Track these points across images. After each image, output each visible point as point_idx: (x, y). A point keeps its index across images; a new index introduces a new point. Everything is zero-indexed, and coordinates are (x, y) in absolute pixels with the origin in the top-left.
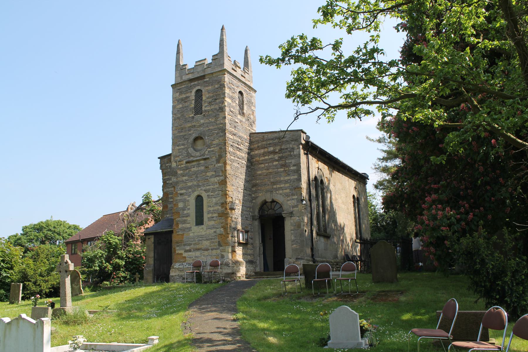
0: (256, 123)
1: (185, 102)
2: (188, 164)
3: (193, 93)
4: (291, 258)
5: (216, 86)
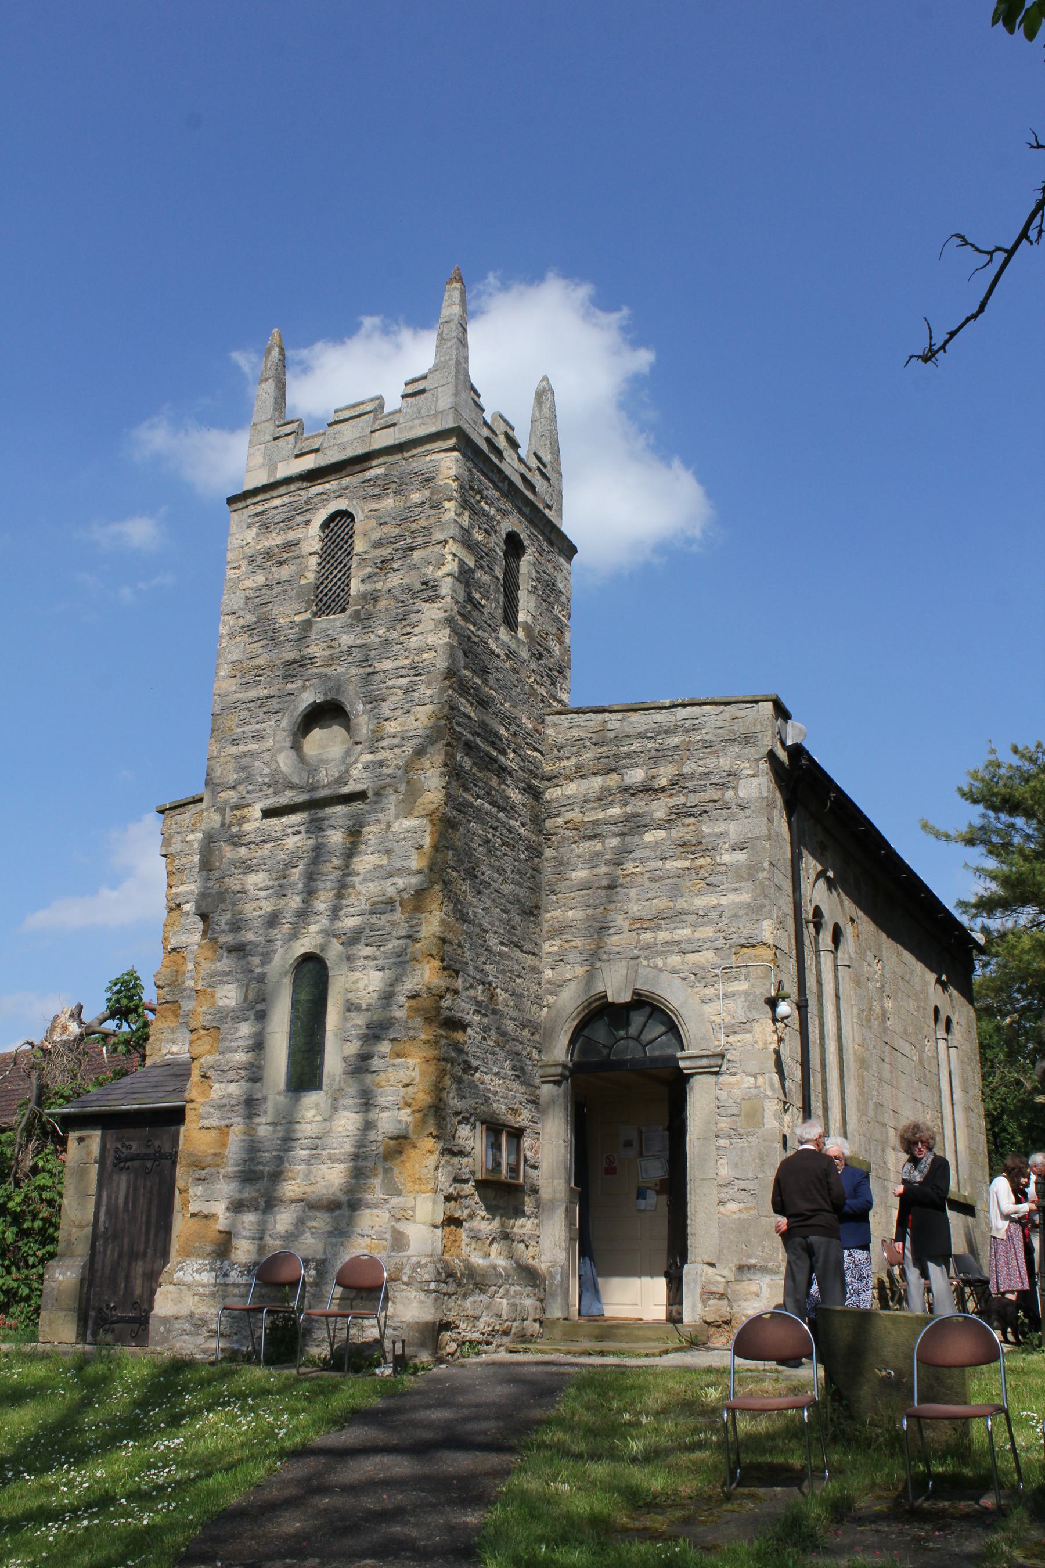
0: (568, 673)
1: (281, 563)
2: (274, 821)
3: (315, 528)
4: (712, 1265)
5: (416, 497)
